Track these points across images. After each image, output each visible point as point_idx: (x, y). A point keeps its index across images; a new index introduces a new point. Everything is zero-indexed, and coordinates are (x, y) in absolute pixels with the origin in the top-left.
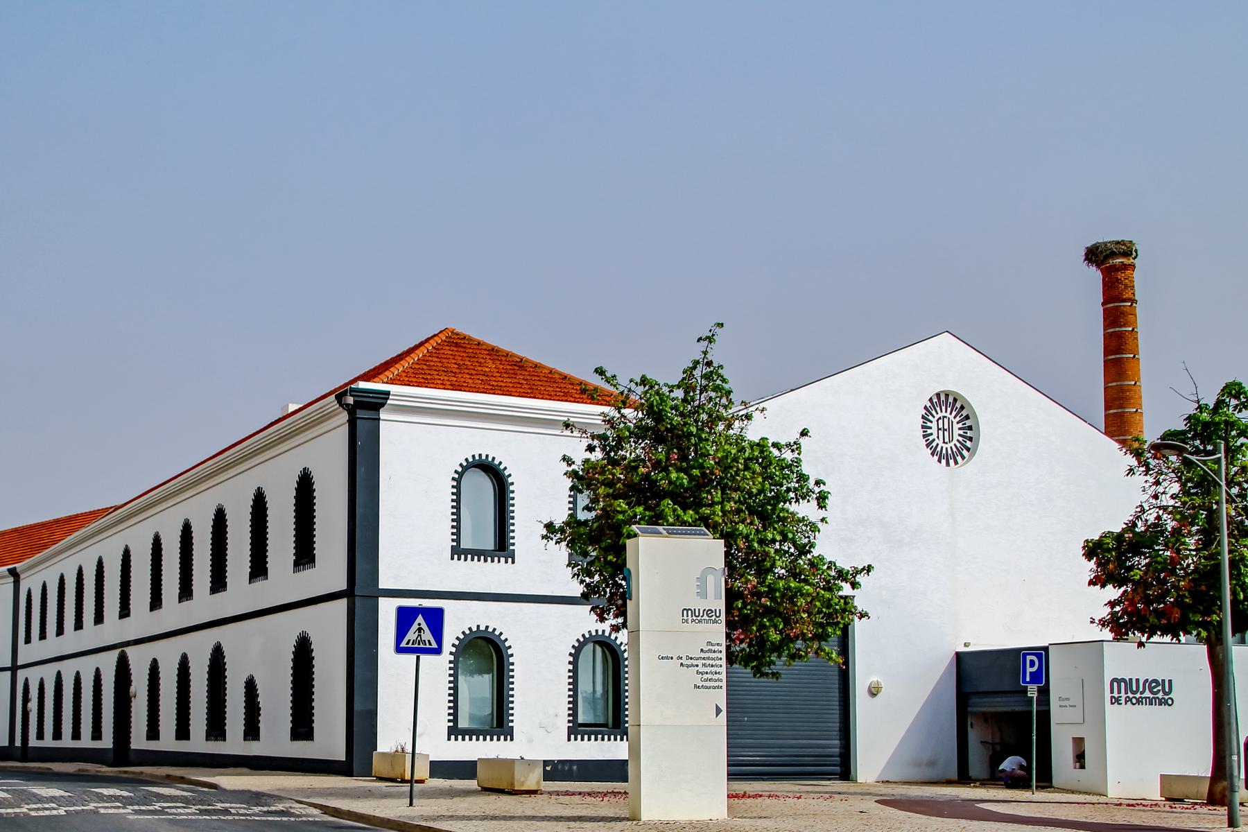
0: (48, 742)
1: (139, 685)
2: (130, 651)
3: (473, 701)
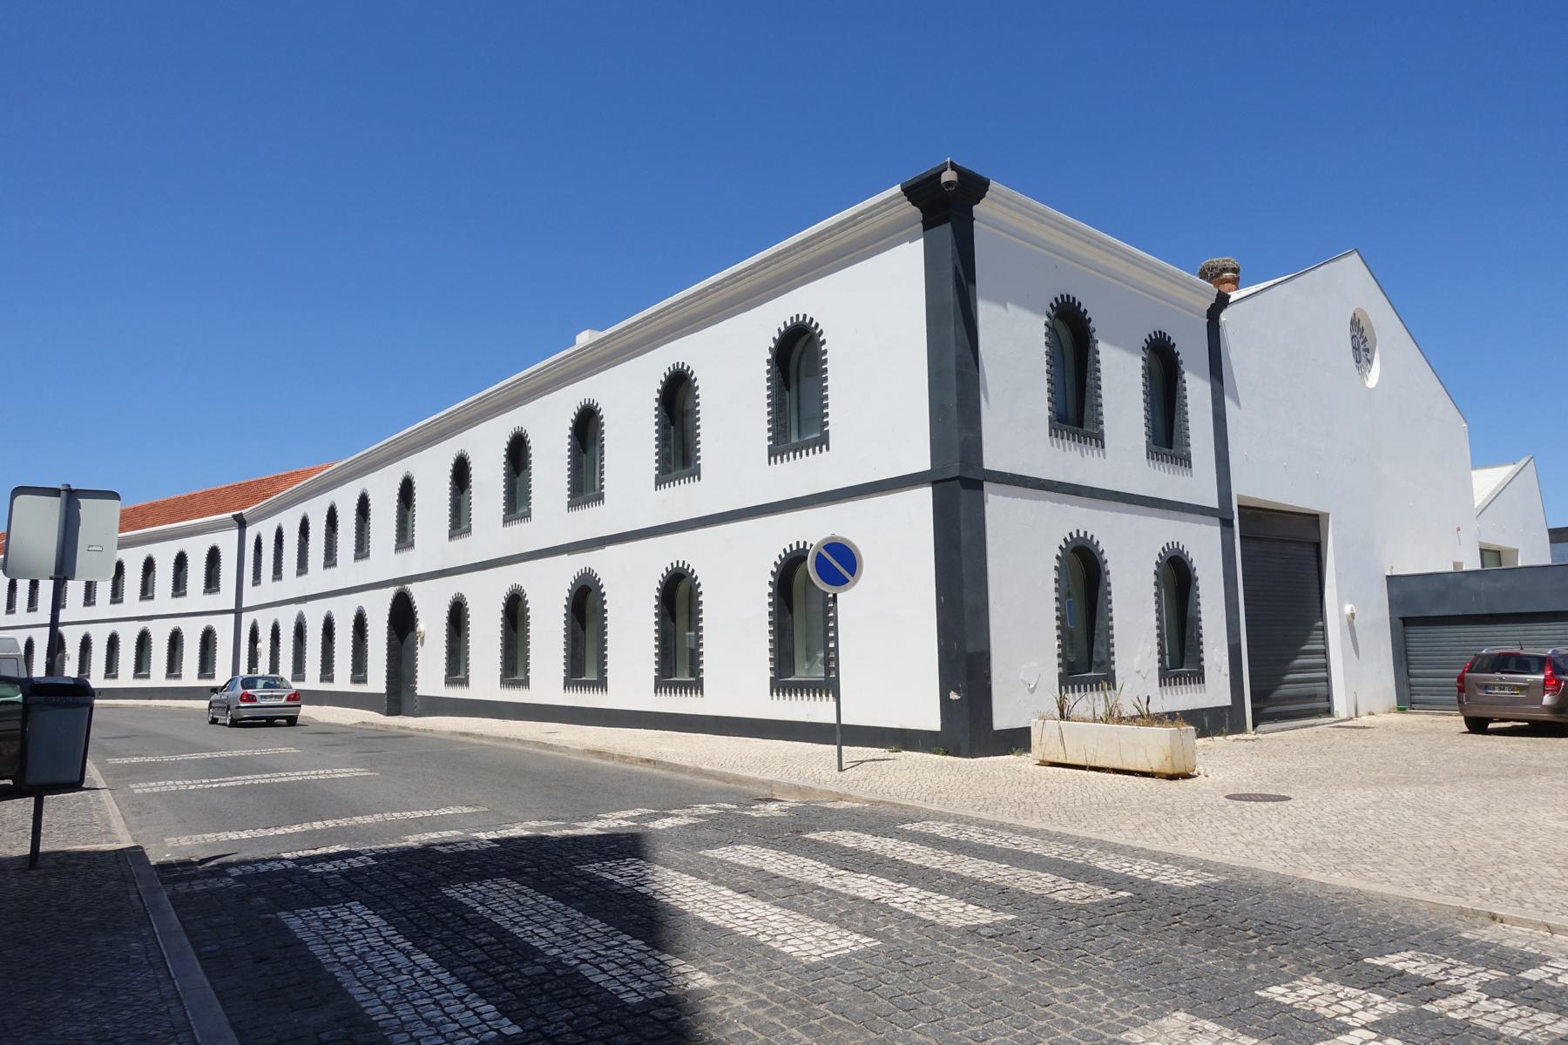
2: (415, 590)
3: (351, 764)
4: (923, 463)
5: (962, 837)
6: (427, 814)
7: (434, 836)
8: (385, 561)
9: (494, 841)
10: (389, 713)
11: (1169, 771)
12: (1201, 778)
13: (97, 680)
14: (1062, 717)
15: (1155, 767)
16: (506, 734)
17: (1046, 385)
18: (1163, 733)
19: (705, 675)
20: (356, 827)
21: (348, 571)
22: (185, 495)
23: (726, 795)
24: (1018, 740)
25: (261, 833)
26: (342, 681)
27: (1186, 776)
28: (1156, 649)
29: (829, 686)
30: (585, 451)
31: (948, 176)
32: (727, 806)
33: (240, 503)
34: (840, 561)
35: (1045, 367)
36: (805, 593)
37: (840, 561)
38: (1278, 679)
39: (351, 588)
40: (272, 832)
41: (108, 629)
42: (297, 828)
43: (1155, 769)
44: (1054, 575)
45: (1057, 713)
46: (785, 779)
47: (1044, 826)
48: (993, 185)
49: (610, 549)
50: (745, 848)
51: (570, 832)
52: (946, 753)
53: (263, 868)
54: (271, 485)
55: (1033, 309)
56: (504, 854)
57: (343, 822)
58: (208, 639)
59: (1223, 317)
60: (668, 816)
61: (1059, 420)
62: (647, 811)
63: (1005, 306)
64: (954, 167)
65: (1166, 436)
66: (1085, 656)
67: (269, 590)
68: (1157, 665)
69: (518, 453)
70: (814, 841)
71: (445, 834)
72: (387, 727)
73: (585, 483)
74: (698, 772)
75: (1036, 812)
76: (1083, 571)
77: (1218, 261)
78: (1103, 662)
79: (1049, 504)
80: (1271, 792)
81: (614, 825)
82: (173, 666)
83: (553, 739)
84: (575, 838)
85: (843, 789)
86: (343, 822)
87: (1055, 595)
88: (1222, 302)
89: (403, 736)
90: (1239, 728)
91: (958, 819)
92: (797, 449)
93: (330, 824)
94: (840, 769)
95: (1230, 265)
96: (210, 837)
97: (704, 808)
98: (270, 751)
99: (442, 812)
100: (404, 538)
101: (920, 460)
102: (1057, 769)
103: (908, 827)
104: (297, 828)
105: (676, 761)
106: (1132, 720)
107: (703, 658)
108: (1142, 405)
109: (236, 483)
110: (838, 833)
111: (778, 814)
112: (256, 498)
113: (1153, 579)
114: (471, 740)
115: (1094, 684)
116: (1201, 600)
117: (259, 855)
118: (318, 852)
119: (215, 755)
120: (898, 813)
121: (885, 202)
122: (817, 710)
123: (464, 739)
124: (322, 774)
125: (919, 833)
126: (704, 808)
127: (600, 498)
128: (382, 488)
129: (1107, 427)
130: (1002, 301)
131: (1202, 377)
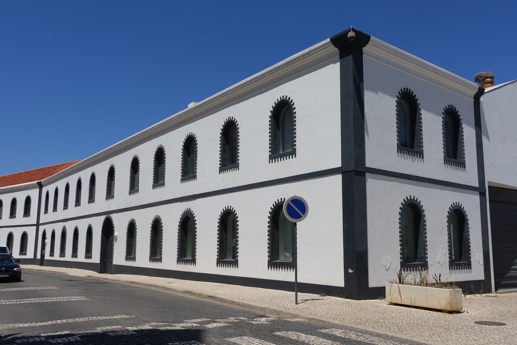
0: (57, 257)
1: (120, 232)
2: (113, 216)
3: (80, 295)
4: (337, 163)
5: (347, 337)
6: (108, 318)
7: (109, 328)
8: (102, 204)
9: (135, 331)
10: (101, 272)
11: (449, 309)
12: (465, 313)
13: (16, 254)
14: (400, 282)
15: (443, 308)
16: (139, 281)
17: (396, 129)
18: (447, 291)
19: (239, 259)
20: (76, 323)
21: (86, 208)
22: (17, 173)
23: (243, 313)
24: (379, 293)
25: (34, 324)
26: (81, 257)
27: (458, 312)
28: (448, 252)
29: (293, 265)
30: (189, 156)
31: (351, 34)
32: (243, 318)
33: (40, 177)
34: (298, 208)
35: (396, 121)
36: (284, 222)
37: (298, 208)
38: (508, 269)
39: (83, 216)
40: (38, 324)
41: (22, 230)
42: (50, 323)
43: (443, 308)
44: (399, 216)
45: (398, 281)
46: (271, 307)
47: (386, 333)
48: (372, 38)
49: (199, 200)
50: (246, 338)
51: (169, 328)
52: (347, 298)
53: (31, 340)
54: (55, 169)
55: (391, 95)
56: (137, 337)
57: (70, 321)
58: (24, 237)
59: (482, 99)
60: (215, 322)
61: (402, 145)
62: (206, 319)
63: (377, 93)
64: (354, 30)
65: (453, 153)
66: (413, 255)
67: (51, 216)
68: (448, 260)
69: (160, 156)
70: (278, 336)
71: (114, 327)
72: (99, 278)
73: (189, 171)
74: (232, 302)
75: (384, 326)
76: (413, 216)
77: (484, 73)
78: (422, 258)
79: (397, 184)
80: (497, 321)
81: (190, 325)
82: (156, 252)
83: (170, 286)
84: (171, 331)
85: (296, 312)
86: (70, 321)
87: (399, 225)
88: (481, 92)
89: (105, 283)
90: (489, 291)
91: (346, 328)
92: (282, 156)
93: (64, 321)
94: (297, 303)
95: (489, 75)
96: (11, 326)
97: (232, 319)
98: (45, 288)
99: (114, 317)
100: (110, 194)
101: (335, 161)
102: (397, 307)
103: (323, 331)
104: (50, 323)
105: (223, 297)
106: (433, 285)
107: (239, 251)
108: (442, 139)
109: (39, 168)
110: (290, 332)
111: (264, 323)
112: (47, 175)
113: (447, 219)
114: (135, 285)
115: (414, 268)
116: (470, 230)
117: (31, 334)
118: (57, 334)
119: (21, 289)
120: (320, 324)
121: (323, 46)
122: (285, 275)
123: (131, 284)
124: (66, 299)
125: (328, 334)
126: (232, 319)
127: (195, 177)
128: (101, 171)
129: (425, 149)
130: (376, 91)
131: (471, 126)
